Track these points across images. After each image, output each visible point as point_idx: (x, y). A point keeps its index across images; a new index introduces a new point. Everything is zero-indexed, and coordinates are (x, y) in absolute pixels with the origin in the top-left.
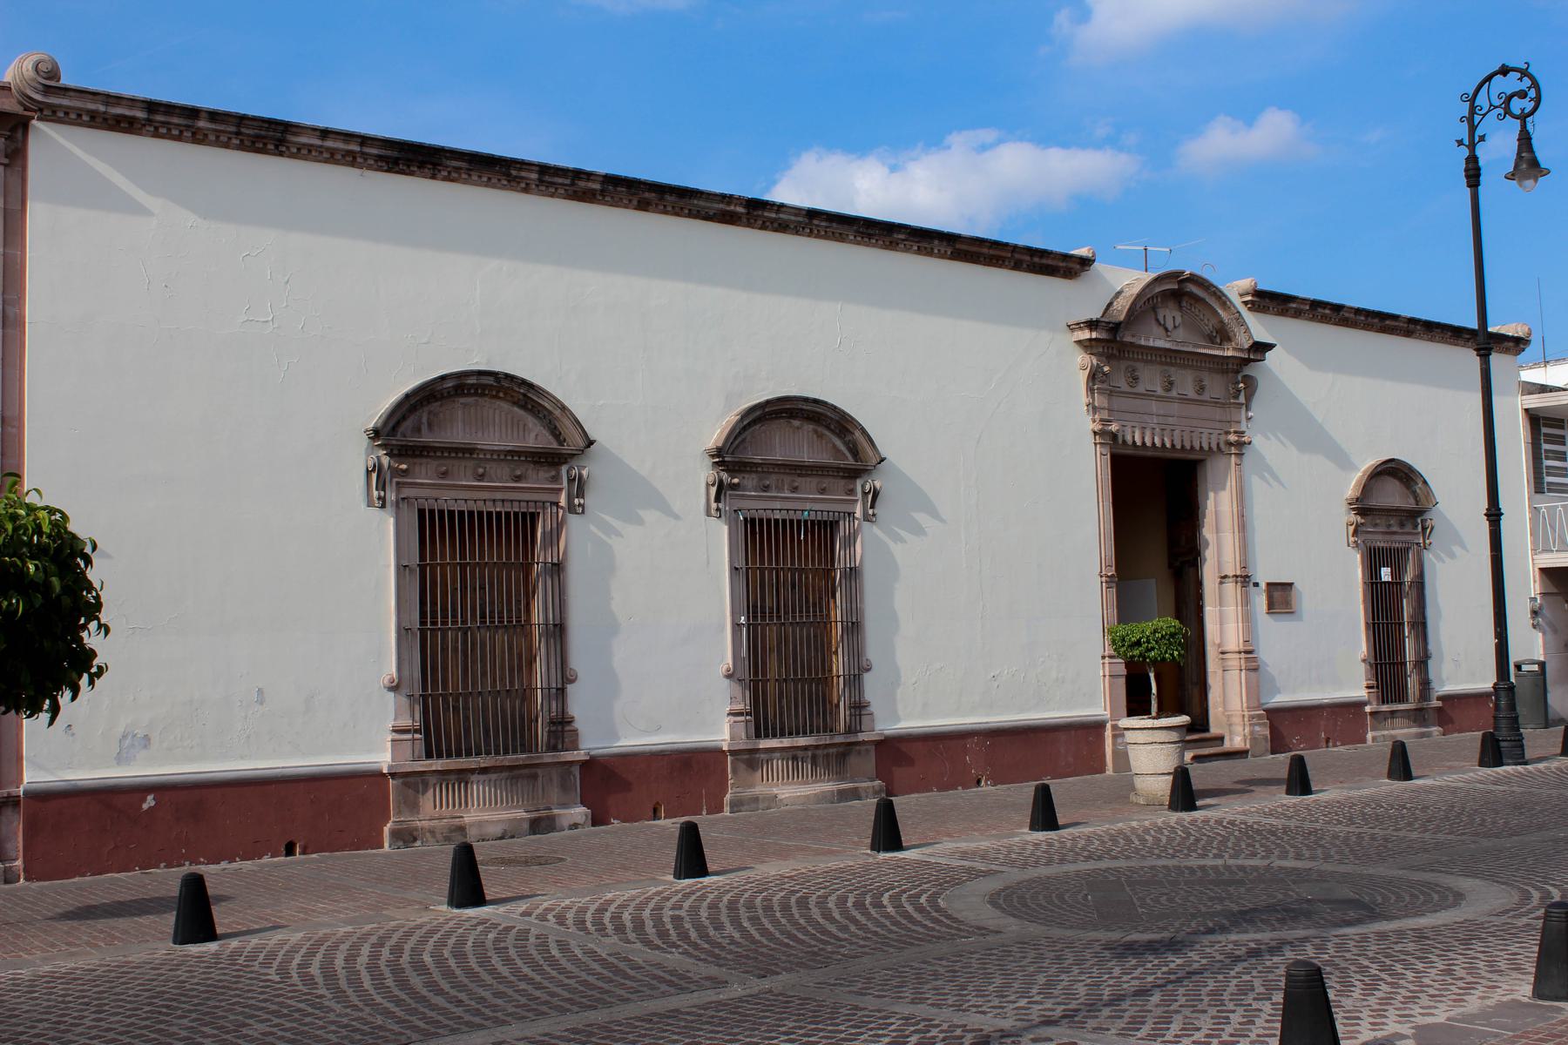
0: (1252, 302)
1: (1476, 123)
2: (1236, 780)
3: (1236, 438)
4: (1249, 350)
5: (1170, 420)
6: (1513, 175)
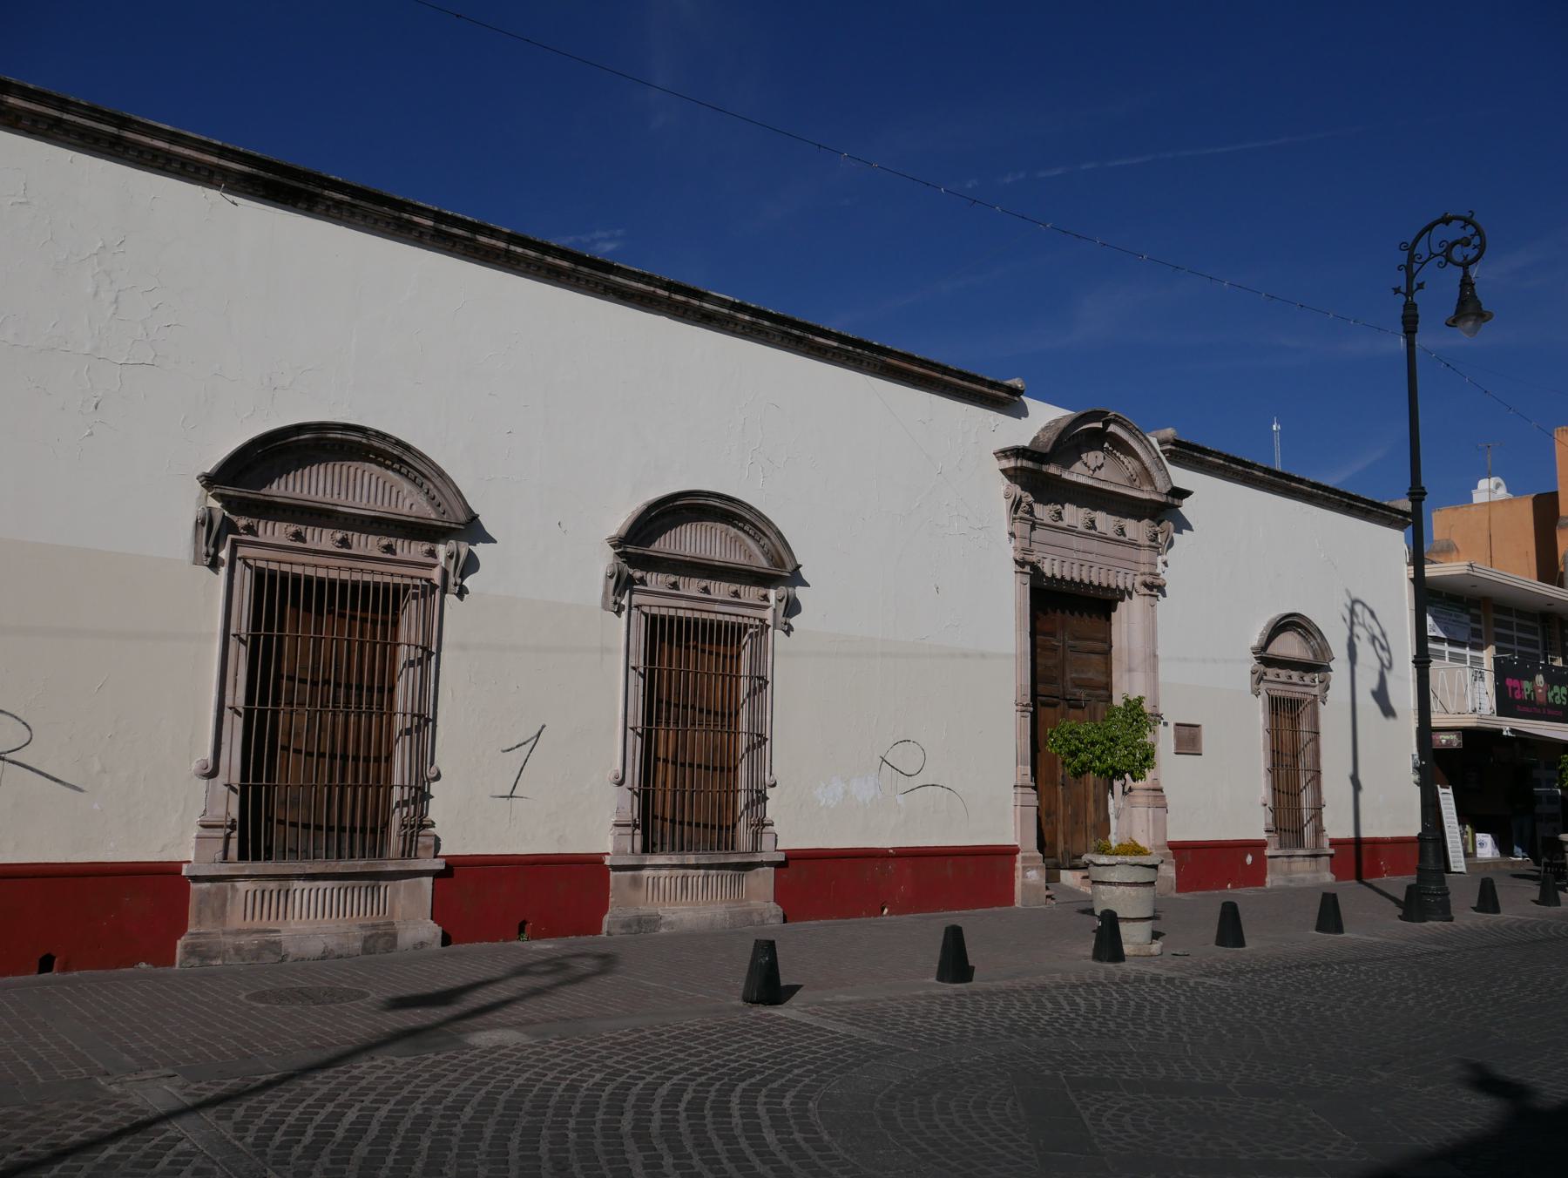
0: (1170, 451)
1: (1414, 271)
2: (1083, 908)
3: (1152, 580)
4: (1168, 494)
5: (1089, 557)
6: (1454, 321)
